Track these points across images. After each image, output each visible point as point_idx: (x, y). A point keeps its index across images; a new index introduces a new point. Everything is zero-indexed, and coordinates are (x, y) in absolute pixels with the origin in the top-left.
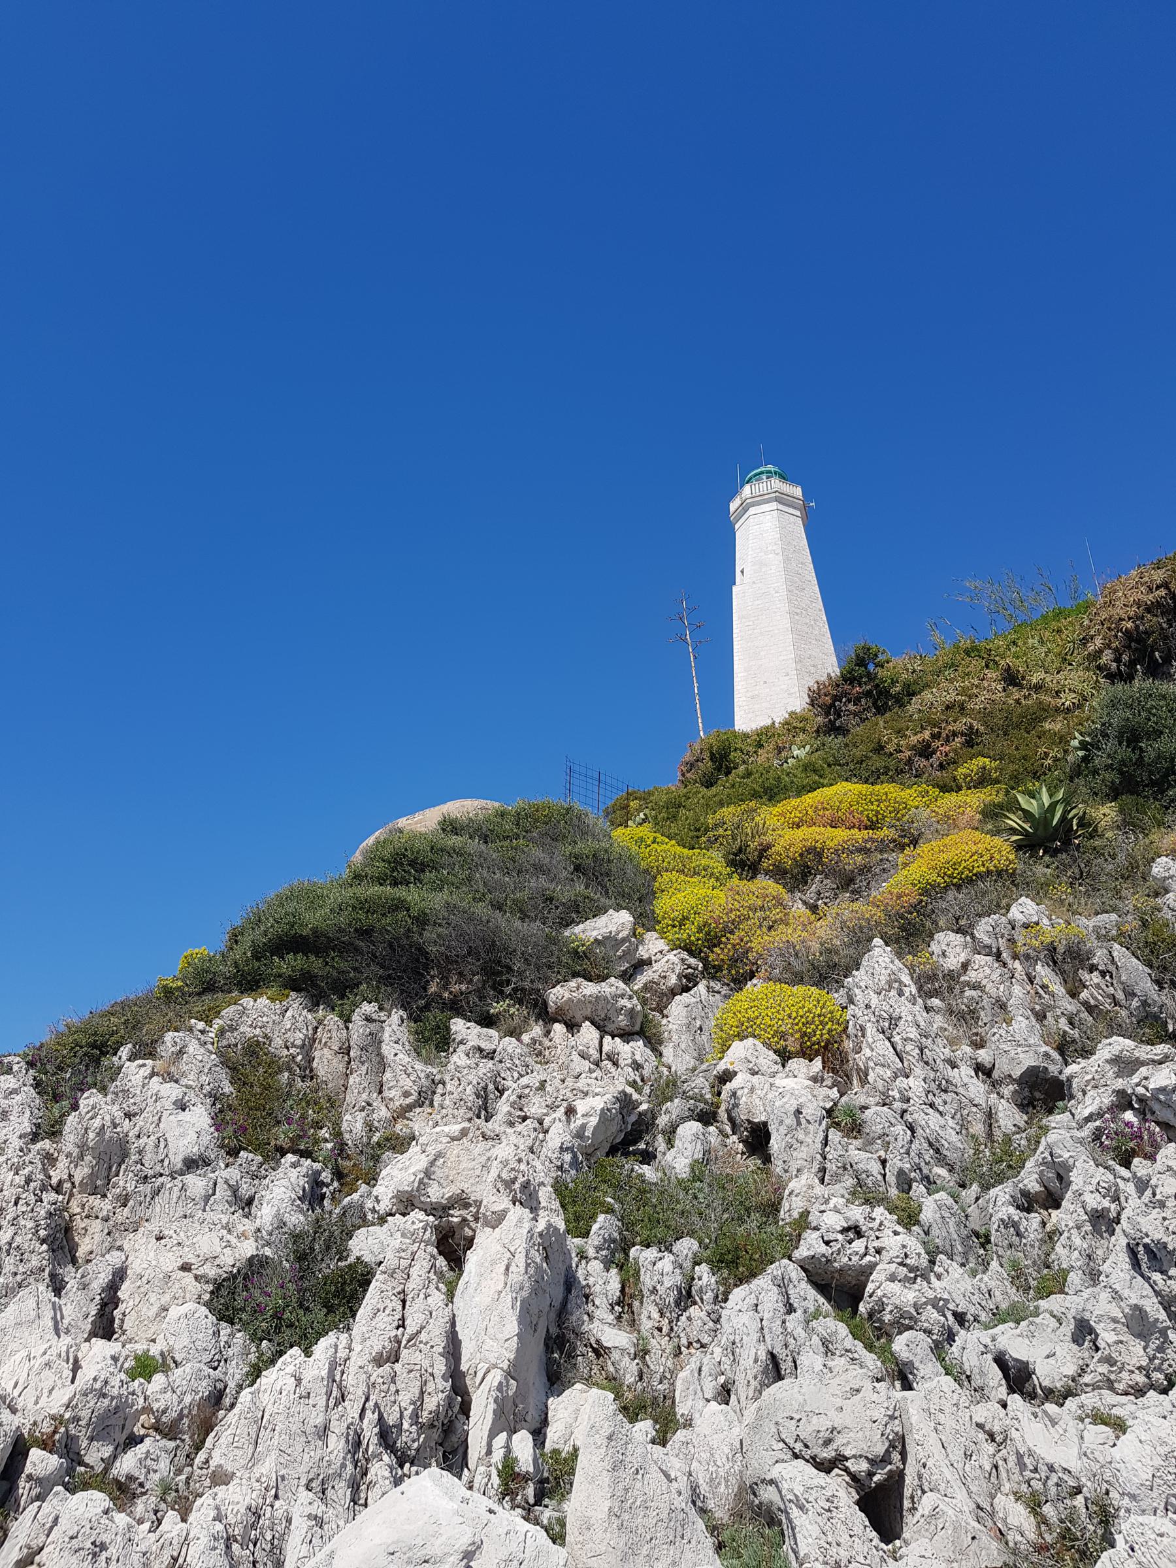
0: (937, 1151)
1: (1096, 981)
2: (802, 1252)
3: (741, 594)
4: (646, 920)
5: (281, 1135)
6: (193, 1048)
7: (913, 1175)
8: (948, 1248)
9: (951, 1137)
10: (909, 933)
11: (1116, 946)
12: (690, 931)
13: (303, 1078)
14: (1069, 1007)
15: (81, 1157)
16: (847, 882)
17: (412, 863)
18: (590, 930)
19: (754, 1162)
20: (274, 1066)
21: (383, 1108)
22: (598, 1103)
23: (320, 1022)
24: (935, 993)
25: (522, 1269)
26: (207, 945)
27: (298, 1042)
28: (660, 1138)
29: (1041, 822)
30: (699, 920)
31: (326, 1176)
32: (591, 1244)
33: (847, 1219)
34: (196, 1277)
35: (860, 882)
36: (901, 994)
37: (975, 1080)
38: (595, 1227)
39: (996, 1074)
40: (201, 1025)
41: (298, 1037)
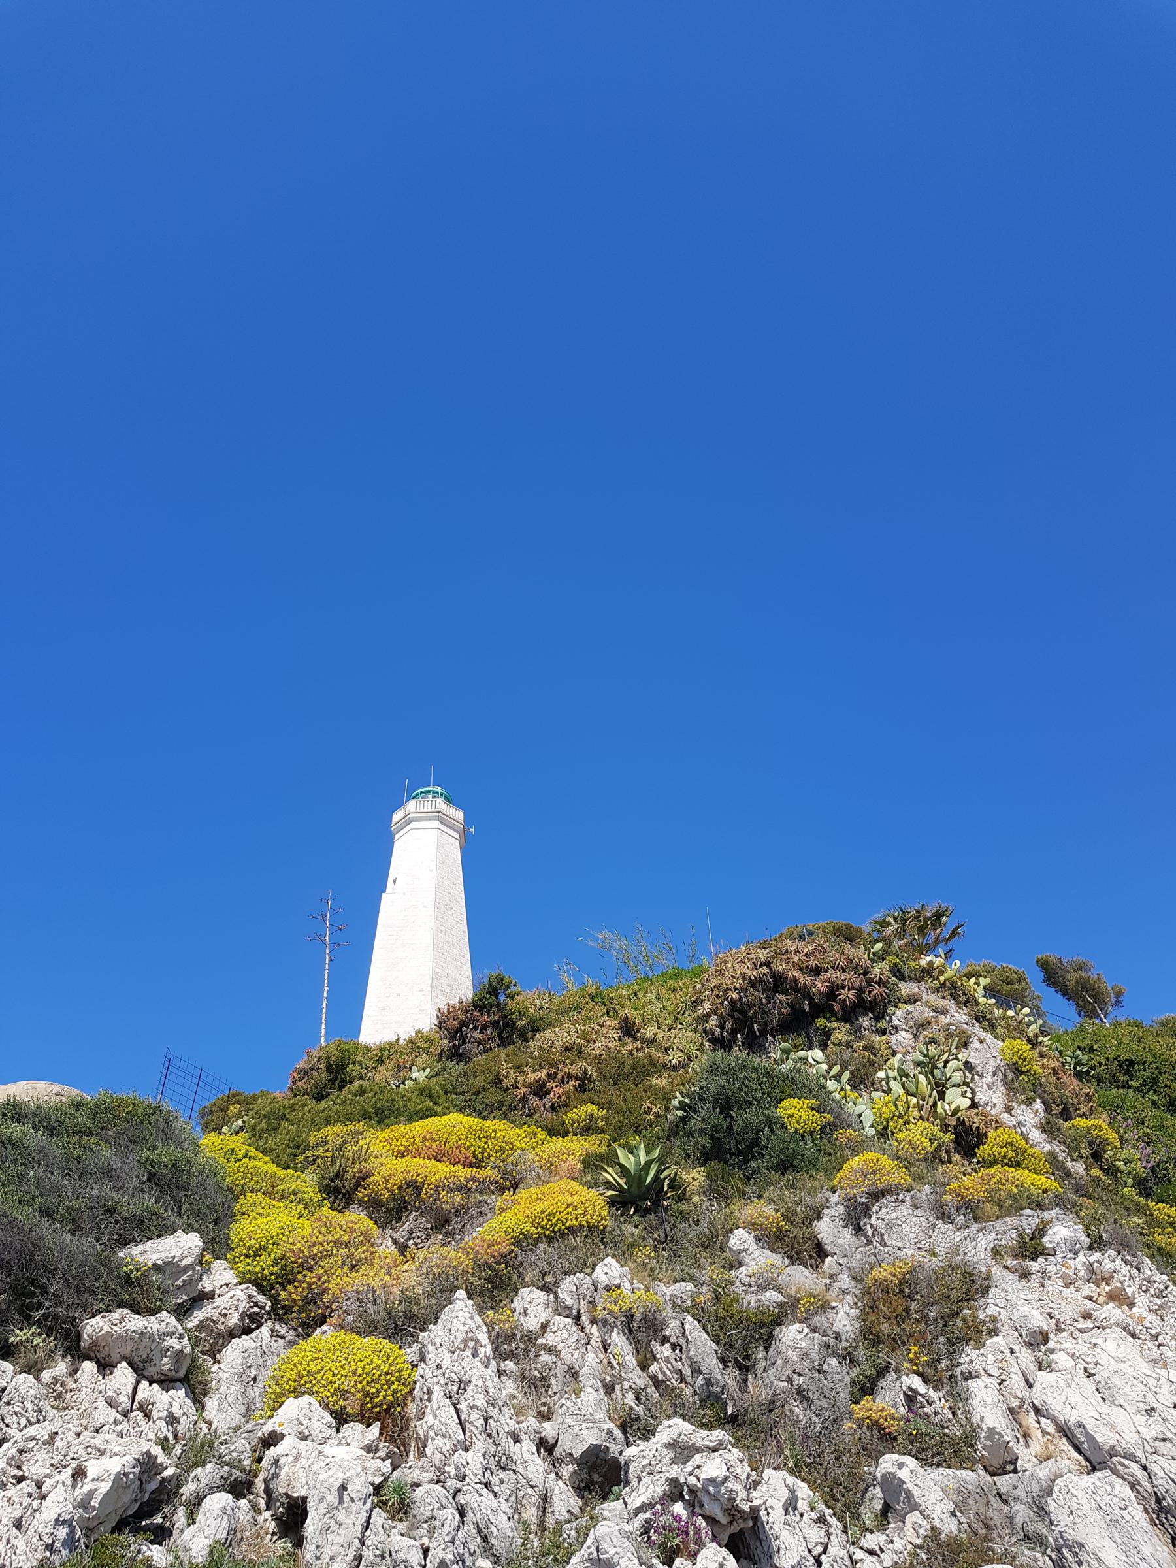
0: (485, 1539)
1: (666, 1354)
4: (217, 1246)
9: (502, 1526)
10: (494, 1286)
12: (265, 1265)
16: (444, 1223)
18: (149, 1253)
22: (114, 1465)
28: (181, 1511)
29: (635, 1178)
30: (277, 1252)
35: (455, 1224)
36: (475, 1355)
39: (557, 1452)
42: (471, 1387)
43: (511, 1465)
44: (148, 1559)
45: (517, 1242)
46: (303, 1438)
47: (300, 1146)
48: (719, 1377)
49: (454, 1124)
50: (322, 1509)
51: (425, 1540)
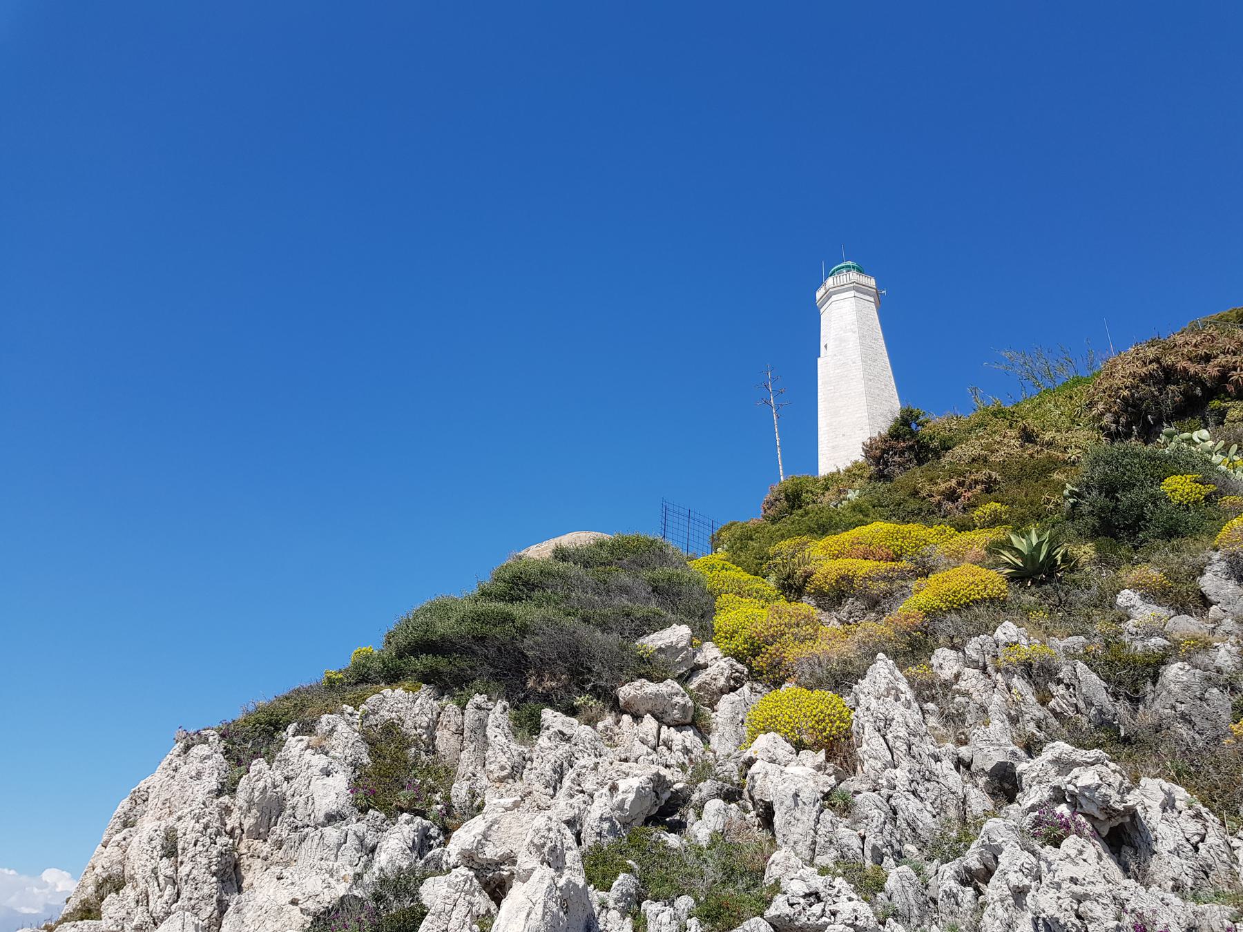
0: (914, 830)
1: (1061, 692)
2: (771, 912)
3: (824, 365)
4: (704, 632)
5: (404, 797)
6: (342, 727)
7: (884, 850)
8: (906, 912)
9: (926, 820)
10: (913, 648)
11: (1080, 663)
12: (738, 643)
13: (427, 753)
14: (1037, 713)
15: (249, 810)
16: (874, 604)
17: (526, 584)
18: (655, 641)
19: (763, 835)
20: (405, 742)
21: (485, 778)
22: (635, 783)
23: (443, 709)
24: (933, 698)
25: (540, 917)
26: (371, 645)
27: (424, 724)
28: (691, 811)
29: (1030, 558)
30: (746, 633)
31: (434, 831)
32: (611, 897)
33: (809, 887)
34: (302, 910)
35: (884, 604)
36: (897, 699)
37: (954, 772)
38: (615, 883)
39: (973, 768)
40: (350, 709)
41: (424, 721)
42: (894, 723)
43: (934, 778)
44: (665, 842)
45: (928, 614)
46: (773, 761)
47: (764, 557)
48: (1110, 707)
49: (878, 529)
50: (783, 809)
51: (862, 831)
